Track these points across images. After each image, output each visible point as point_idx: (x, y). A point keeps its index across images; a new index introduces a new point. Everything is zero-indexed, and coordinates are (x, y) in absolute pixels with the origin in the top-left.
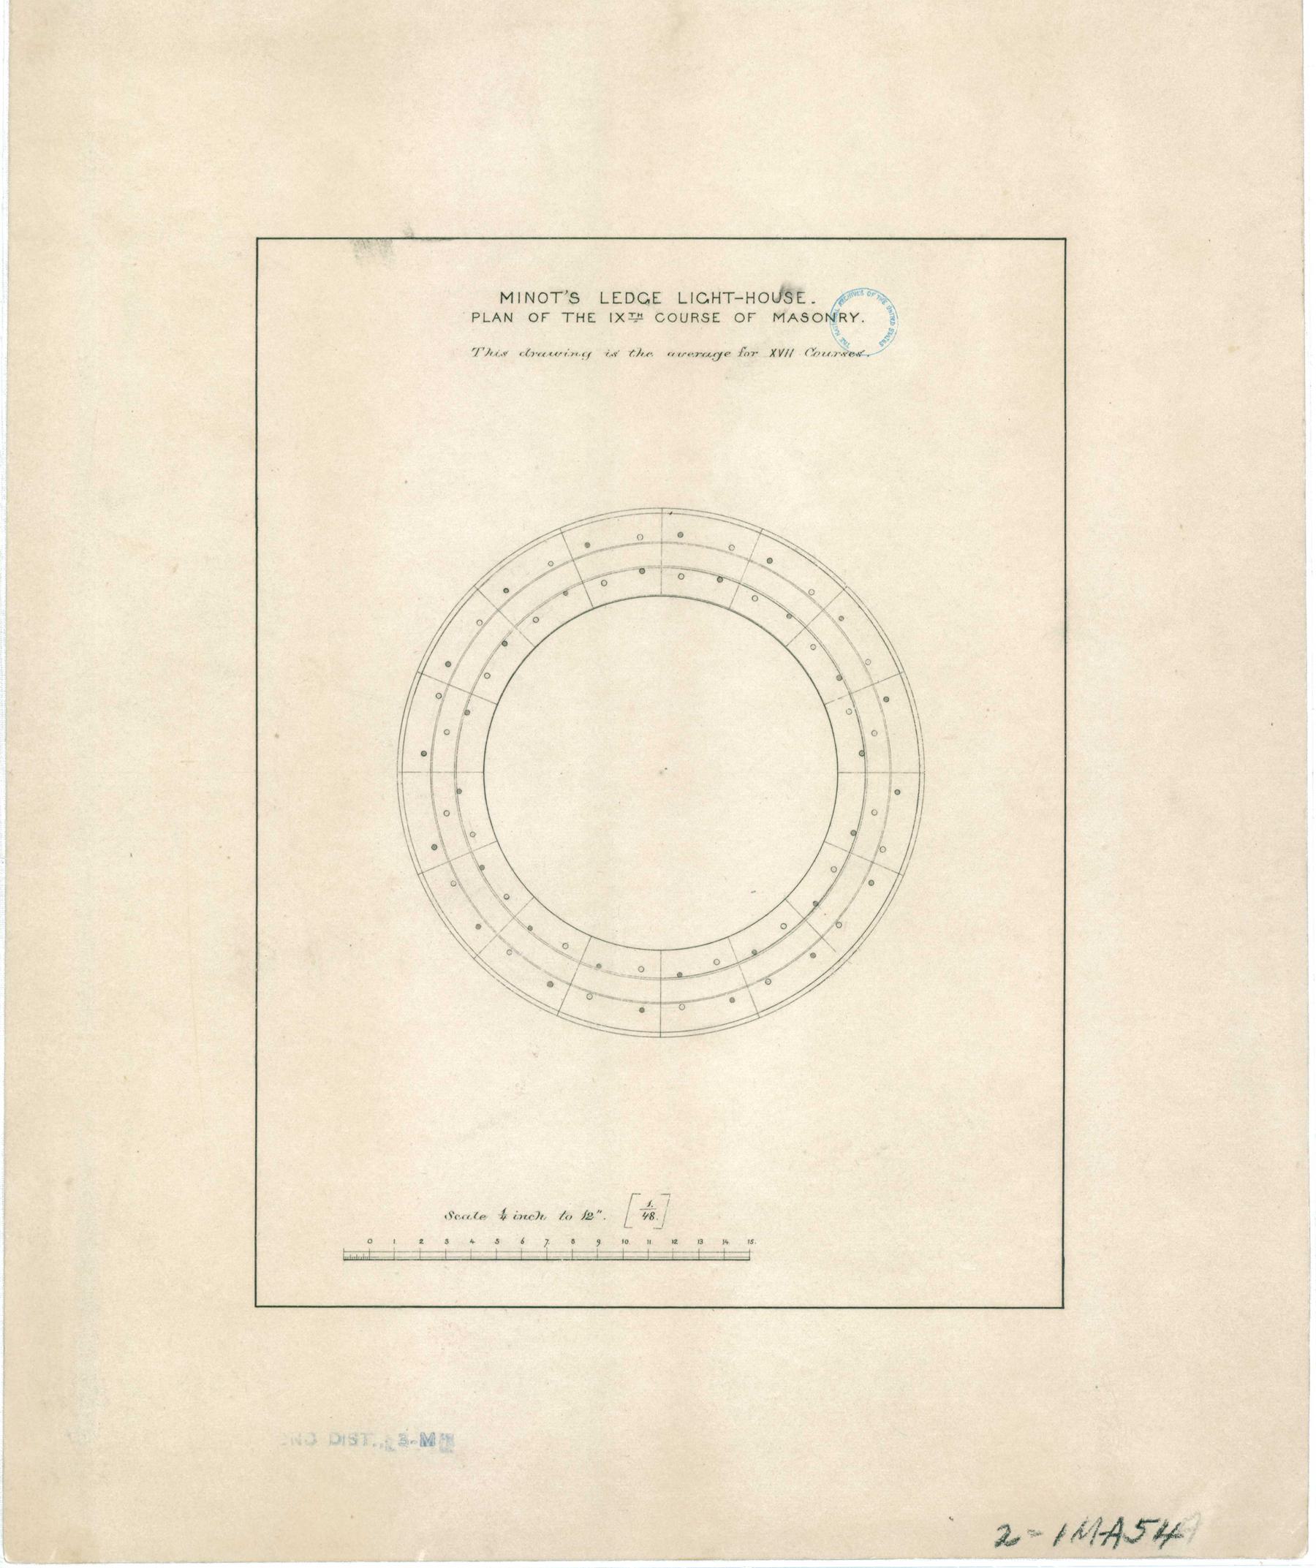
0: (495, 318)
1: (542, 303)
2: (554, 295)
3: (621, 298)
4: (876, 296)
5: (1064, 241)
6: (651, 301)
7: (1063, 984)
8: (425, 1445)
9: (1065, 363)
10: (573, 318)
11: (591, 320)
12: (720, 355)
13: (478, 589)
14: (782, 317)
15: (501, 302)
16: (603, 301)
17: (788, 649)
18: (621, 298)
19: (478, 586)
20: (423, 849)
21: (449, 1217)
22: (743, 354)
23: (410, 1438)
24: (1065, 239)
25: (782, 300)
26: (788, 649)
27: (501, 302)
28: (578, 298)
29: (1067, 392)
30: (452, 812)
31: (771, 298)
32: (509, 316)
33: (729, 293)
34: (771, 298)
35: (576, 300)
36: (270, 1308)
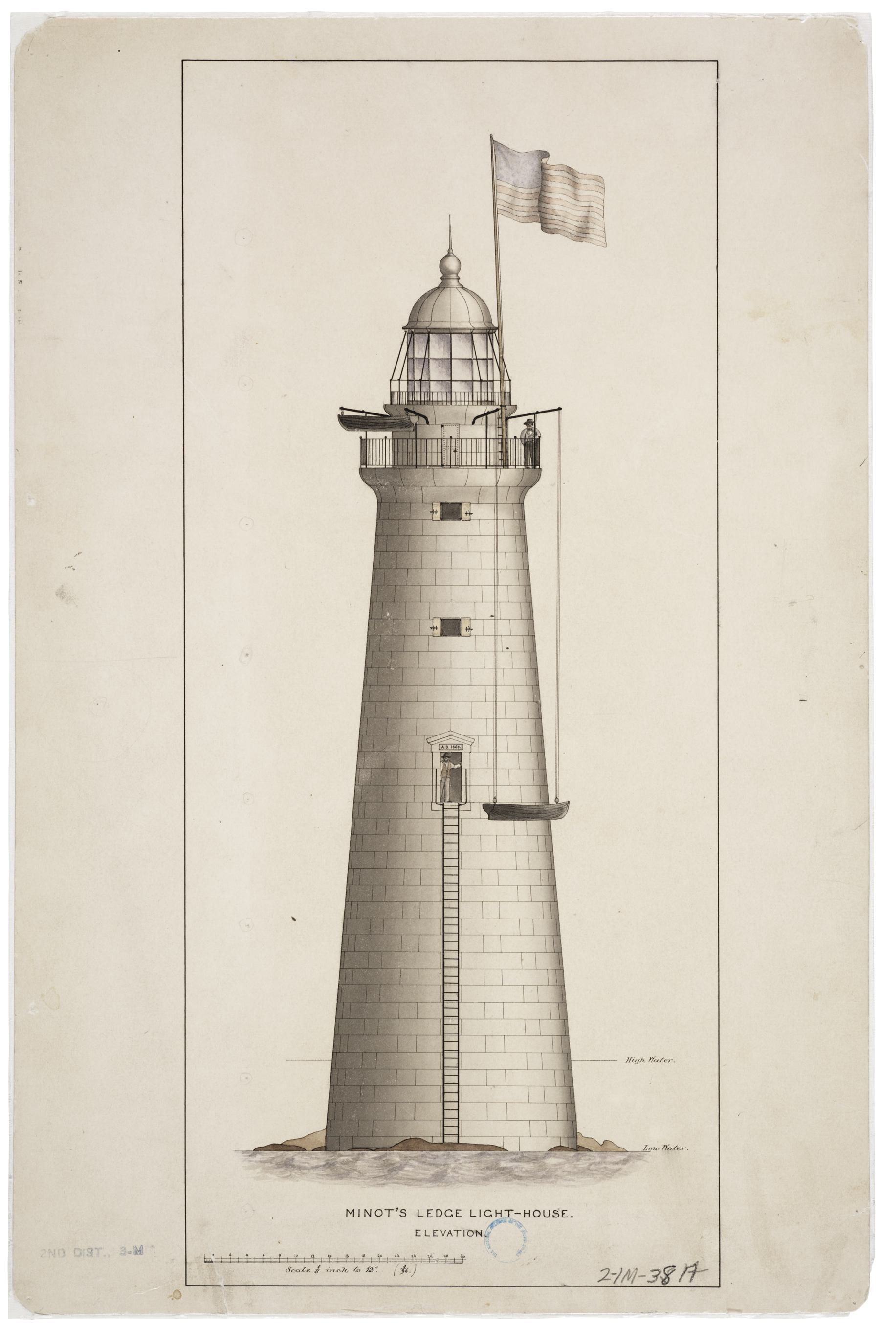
0: (449, 1233)
2: (507, 1211)
3: (433, 1213)
4: (514, 1223)
6: (454, 1215)
9: (283, 60)
10: (461, 1233)
11: (429, 1215)
13: (432, 802)
14: (352, 1213)
15: (371, 1210)
18: (433, 1213)
19: (474, 331)
20: (432, 1157)
21: (288, 1270)
23: (128, 1250)
24: (183, 61)
25: (551, 1216)
27: (347, 1216)
28: (405, 1213)
30: (481, 627)
31: (542, 1213)
33: (389, 1210)
34: (542, 1213)
35: (402, 1211)
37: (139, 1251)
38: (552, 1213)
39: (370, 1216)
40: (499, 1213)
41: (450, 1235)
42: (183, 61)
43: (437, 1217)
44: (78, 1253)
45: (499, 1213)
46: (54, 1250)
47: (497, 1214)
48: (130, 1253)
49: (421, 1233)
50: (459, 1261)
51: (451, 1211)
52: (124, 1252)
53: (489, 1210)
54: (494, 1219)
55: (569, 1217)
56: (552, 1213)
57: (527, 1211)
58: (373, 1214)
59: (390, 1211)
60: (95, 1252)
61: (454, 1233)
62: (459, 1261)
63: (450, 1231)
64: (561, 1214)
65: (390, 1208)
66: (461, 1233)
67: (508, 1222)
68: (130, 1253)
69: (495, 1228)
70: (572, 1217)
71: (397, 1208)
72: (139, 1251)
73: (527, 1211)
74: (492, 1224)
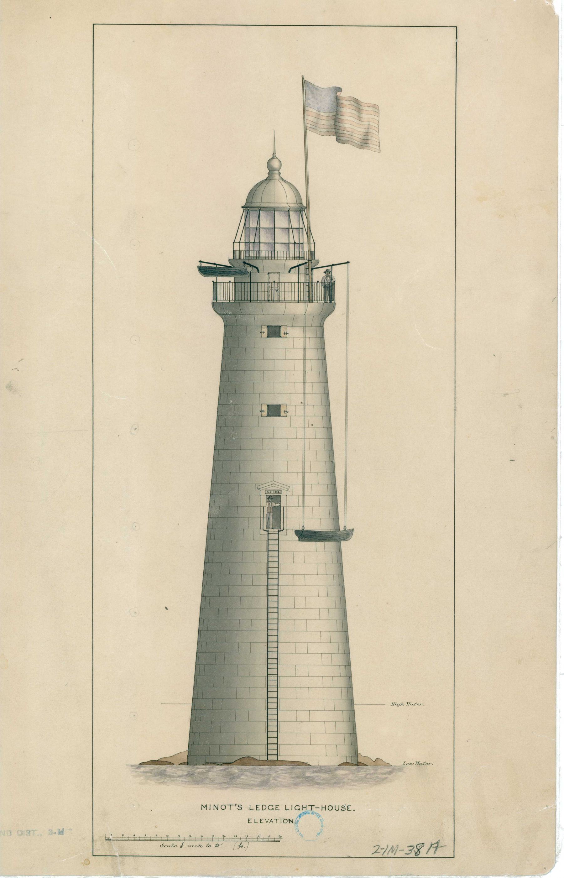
0: (271, 821)
1: (295, 808)
3: (260, 807)
4: (315, 815)
5: (456, 28)
6: (275, 809)
7: (94, 633)
8: (60, 834)
12: (172, 846)
14: (206, 807)
15: (202, 809)
16: (251, 809)
17: (278, 622)
22: (208, 846)
24: (93, 24)
26: (278, 622)
27: (202, 809)
29: (94, 143)
32: (291, 822)
36: (453, 741)
37: (61, 832)
38: (340, 808)
39: (218, 809)
40: (305, 808)
41: (271, 822)
42: (93, 24)
43: (263, 810)
44: (20, 833)
45: (305, 808)
46: (4, 831)
47: (304, 808)
48: (55, 833)
49: (252, 821)
50: (278, 840)
51: (273, 806)
52: (51, 833)
53: (298, 806)
54: (301, 811)
55: (352, 810)
56: (340, 808)
57: (324, 806)
58: (219, 808)
59: (231, 806)
60: (32, 832)
61: (274, 821)
62: (278, 840)
63: (271, 819)
64: (346, 808)
65: (231, 804)
66: (279, 821)
67: (311, 814)
68: (55, 833)
69: (302, 818)
70: (354, 810)
71: (236, 804)
72: (61, 832)
73: (324, 806)
74: (300, 815)
